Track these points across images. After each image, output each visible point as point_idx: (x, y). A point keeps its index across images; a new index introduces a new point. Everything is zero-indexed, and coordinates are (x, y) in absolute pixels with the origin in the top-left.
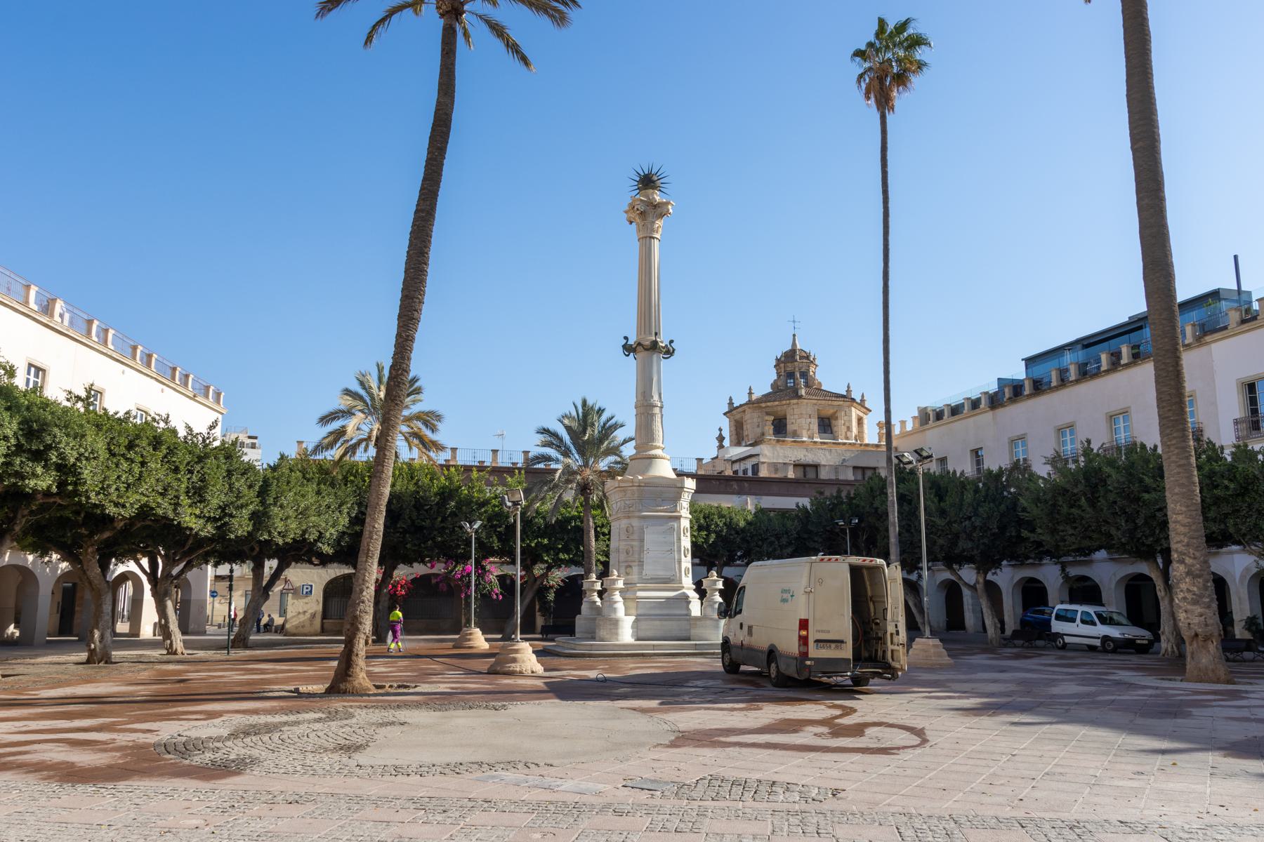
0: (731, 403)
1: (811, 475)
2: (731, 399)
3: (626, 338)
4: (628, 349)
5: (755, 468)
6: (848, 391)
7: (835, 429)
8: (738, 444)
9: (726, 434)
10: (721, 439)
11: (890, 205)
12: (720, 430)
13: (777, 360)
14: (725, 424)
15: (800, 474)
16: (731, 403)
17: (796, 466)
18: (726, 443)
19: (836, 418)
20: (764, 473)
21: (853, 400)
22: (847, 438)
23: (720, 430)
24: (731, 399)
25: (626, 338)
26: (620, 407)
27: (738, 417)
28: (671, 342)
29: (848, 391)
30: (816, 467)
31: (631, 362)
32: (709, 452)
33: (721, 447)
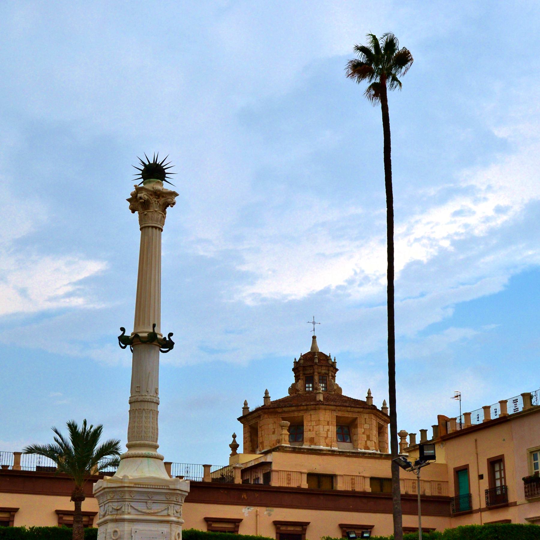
0: (267, 397)
1: (326, 486)
2: (266, 393)
3: (123, 329)
4: (124, 341)
5: (267, 477)
6: (369, 397)
7: (355, 438)
8: (253, 451)
9: (240, 440)
10: (234, 446)
11: (394, 205)
12: (234, 436)
13: (295, 363)
14: (239, 429)
15: (314, 486)
16: (246, 408)
17: (310, 476)
18: (240, 450)
19: (356, 426)
20: (275, 482)
21: (374, 407)
22: (367, 448)
23: (234, 436)
24: (266, 393)
25: (123, 329)
26: (115, 430)
27: (253, 422)
28: (171, 335)
29: (369, 397)
30: (332, 478)
31: (127, 353)
32: (220, 460)
33: (234, 453)
